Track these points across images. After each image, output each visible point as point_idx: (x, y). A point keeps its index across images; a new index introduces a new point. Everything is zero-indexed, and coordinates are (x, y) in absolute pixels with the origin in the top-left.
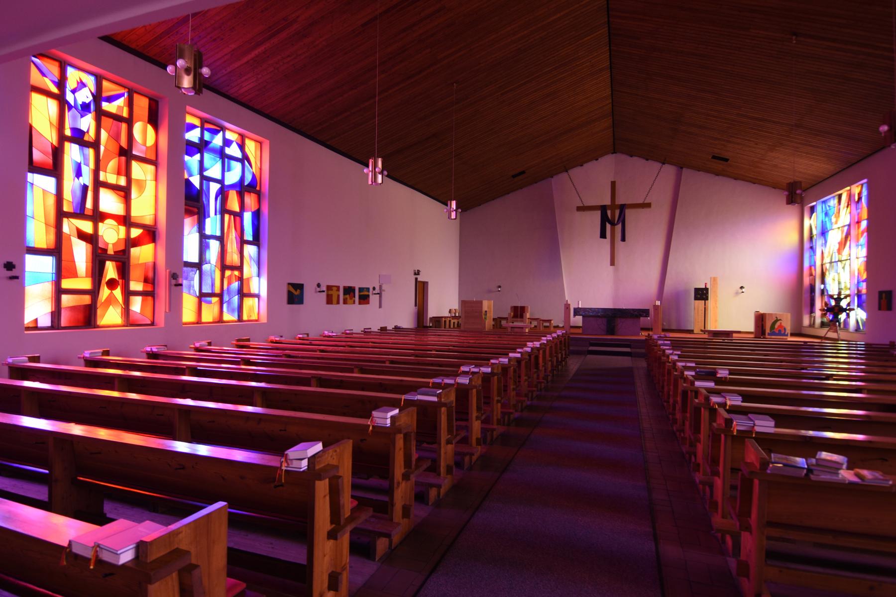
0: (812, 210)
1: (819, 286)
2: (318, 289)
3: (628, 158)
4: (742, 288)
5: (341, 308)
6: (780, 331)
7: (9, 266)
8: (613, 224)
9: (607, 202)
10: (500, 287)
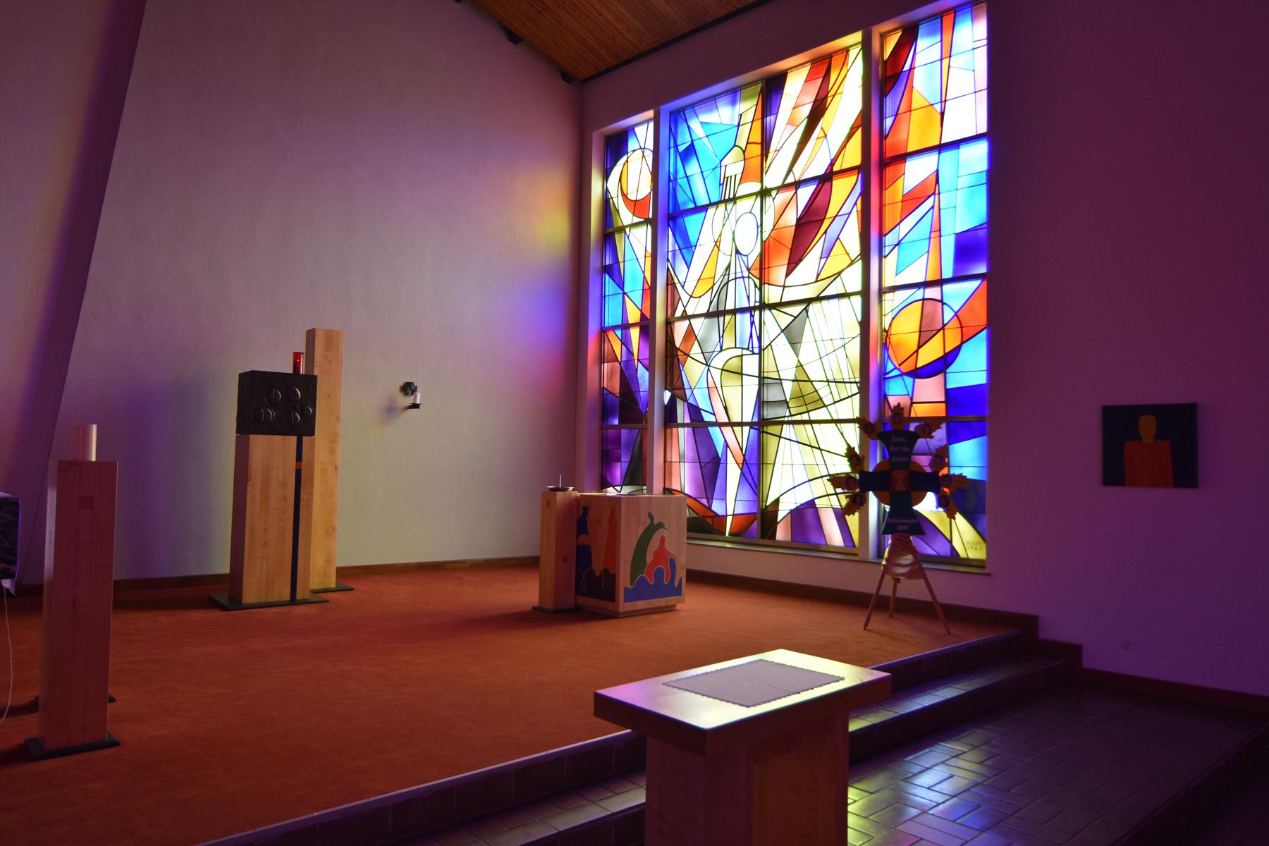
4: (408, 389)
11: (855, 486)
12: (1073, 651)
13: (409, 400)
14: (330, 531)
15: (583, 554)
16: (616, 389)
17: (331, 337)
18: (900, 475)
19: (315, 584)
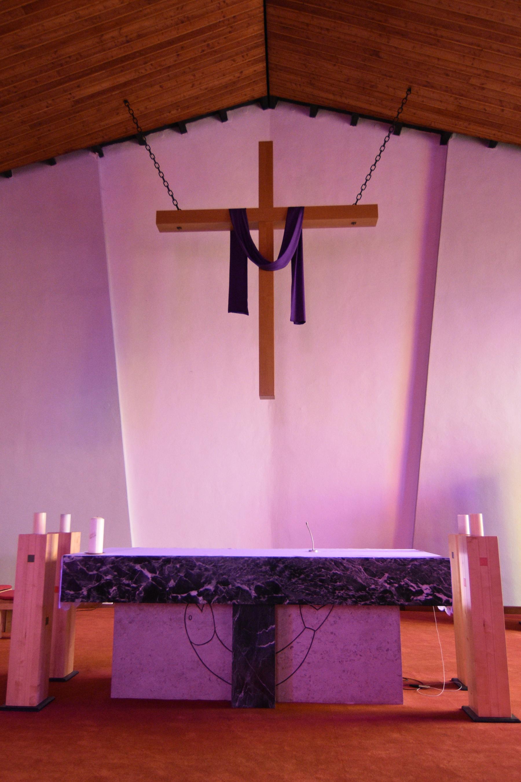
7: (92, 519)
8: (267, 265)
9: (250, 201)
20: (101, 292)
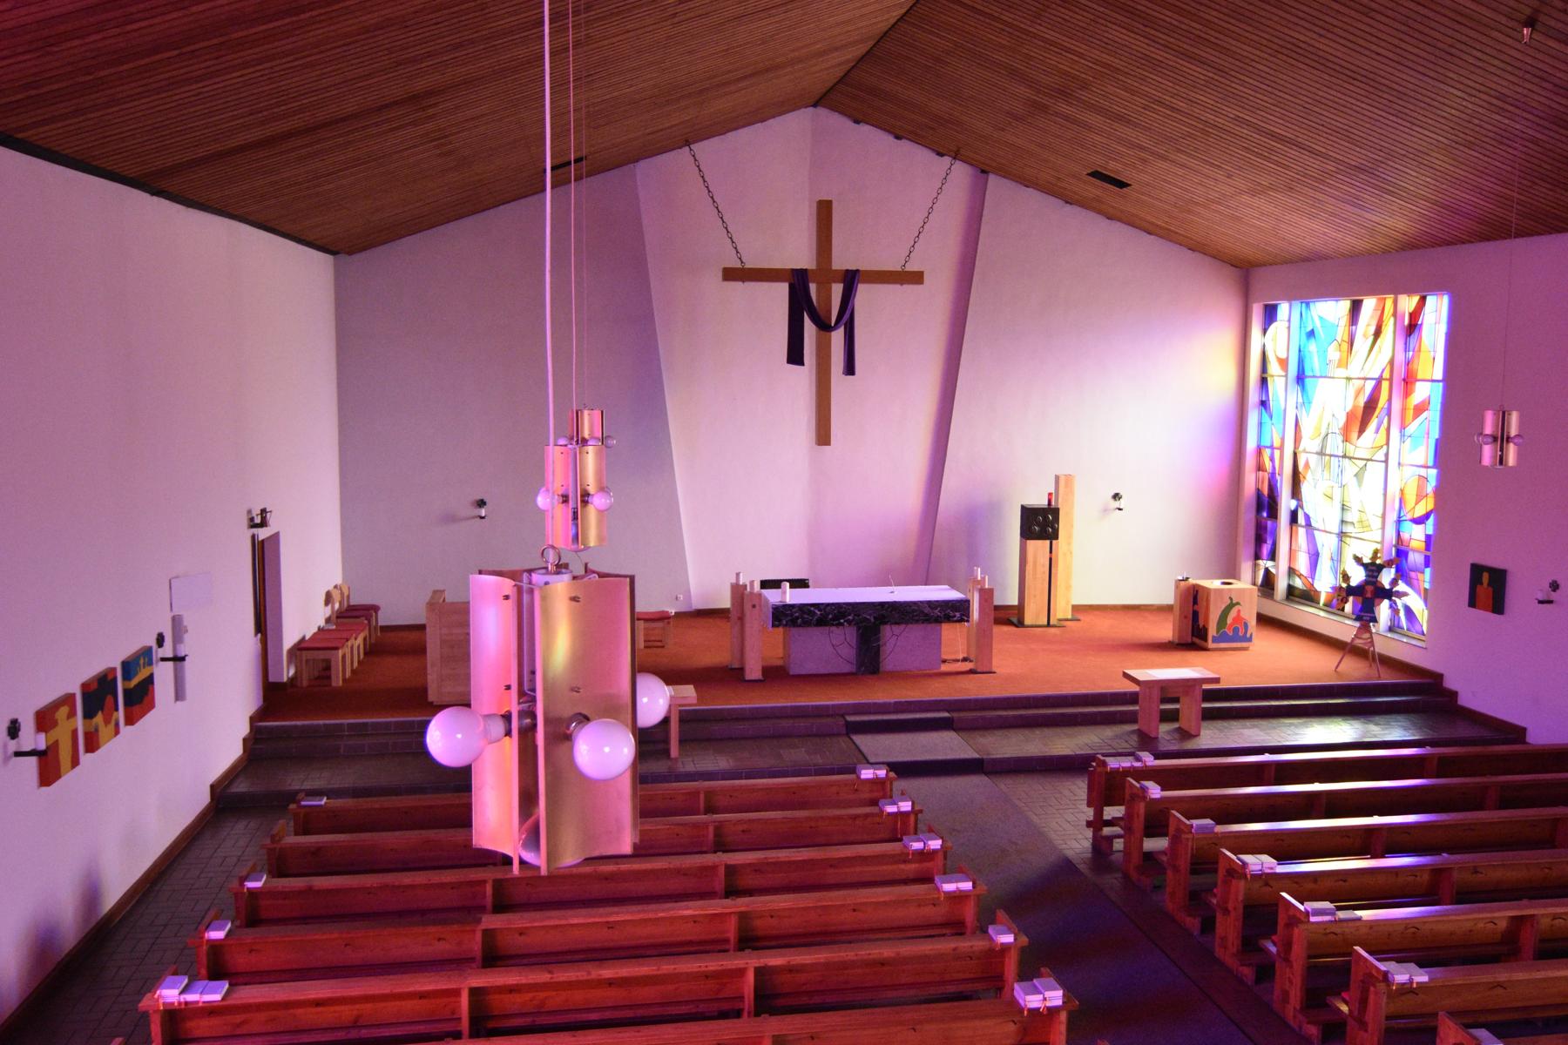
0: (1270, 314)
1: (1286, 504)
2: (13, 746)
3: (849, 124)
4: (1116, 496)
5: (91, 774)
6: (1236, 630)
8: (824, 326)
9: (801, 256)
10: (481, 503)
11: (1345, 592)
12: (1453, 695)
13: (1117, 504)
14: (1068, 587)
15: (1195, 615)
16: (1266, 492)
17: (1069, 478)
18: (1369, 588)
19: (1060, 616)
20: (649, 317)
